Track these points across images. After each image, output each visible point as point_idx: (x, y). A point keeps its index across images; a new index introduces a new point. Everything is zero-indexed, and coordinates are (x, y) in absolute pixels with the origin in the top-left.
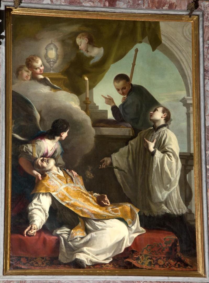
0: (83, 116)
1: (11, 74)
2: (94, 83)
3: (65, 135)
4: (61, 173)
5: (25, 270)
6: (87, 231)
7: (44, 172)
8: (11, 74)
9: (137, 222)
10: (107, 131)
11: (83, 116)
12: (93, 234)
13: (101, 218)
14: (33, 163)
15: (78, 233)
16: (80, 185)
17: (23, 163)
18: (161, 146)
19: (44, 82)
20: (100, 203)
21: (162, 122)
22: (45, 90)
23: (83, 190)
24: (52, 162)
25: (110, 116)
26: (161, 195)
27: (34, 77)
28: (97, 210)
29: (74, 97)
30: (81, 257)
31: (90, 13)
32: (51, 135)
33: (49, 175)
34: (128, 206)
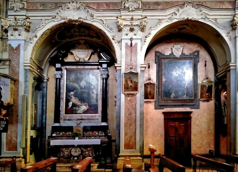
0: (78, 87)
1: (99, 83)
2: (81, 81)
3: (75, 91)
4: (74, 98)
5: (177, 59)
6: (79, 108)
7: (71, 98)
8: (99, 83)
9: (88, 106)
10: (82, 90)
11: (78, 87)
12: (80, 108)
13: (82, 105)
14: (69, 96)
15: (77, 108)
16: (78, 100)
17: (68, 97)
18: (93, 93)
19: (71, 82)
20: (81, 103)
21: (93, 88)
22: (72, 83)
23: (78, 100)
24: (73, 96)
25: (83, 87)
26: (92, 101)
27: (70, 81)
28: (80, 104)
29: (77, 84)
30: (77, 112)
31: (182, 106)
32: (73, 91)
33: (72, 98)
34: (86, 103)
